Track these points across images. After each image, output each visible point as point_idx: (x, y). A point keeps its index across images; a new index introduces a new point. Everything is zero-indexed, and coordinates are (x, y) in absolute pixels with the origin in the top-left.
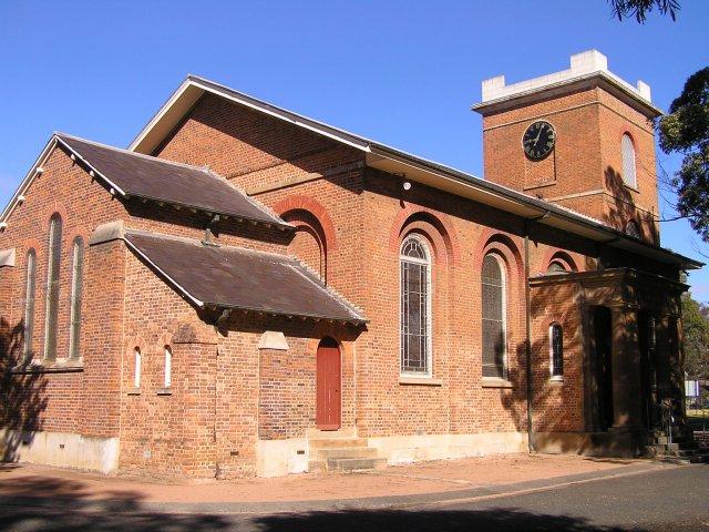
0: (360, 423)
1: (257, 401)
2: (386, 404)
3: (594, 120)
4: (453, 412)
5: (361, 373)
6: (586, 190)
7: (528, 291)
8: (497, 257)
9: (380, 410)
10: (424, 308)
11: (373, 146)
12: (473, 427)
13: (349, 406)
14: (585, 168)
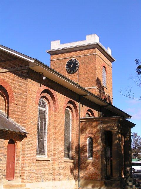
0: (23, 177)
1: (26, 169)
2: (32, 169)
3: (94, 60)
4: (54, 172)
5: (23, 156)
6: (90, 86)
7: (79, 124)
8: (69, 109)
10: (45, 129)
11: (36, 61)
12: (61, 178)
13: (18, 170)
14: (90, 78)
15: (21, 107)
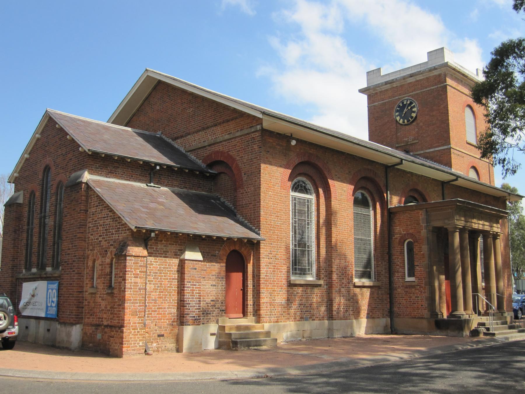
15: (254, 196)
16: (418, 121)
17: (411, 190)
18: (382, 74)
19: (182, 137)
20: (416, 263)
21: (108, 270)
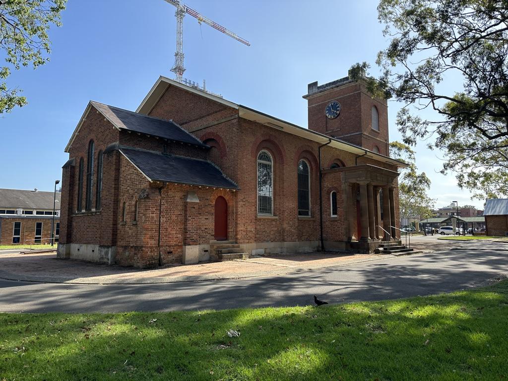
6: (354, 132)
9: (246, 231)
16: (342, 114)
17: (335, 159)
18: (319, 85)
19: (186, 123)
20: (338, 206)
21: (133, 209)
